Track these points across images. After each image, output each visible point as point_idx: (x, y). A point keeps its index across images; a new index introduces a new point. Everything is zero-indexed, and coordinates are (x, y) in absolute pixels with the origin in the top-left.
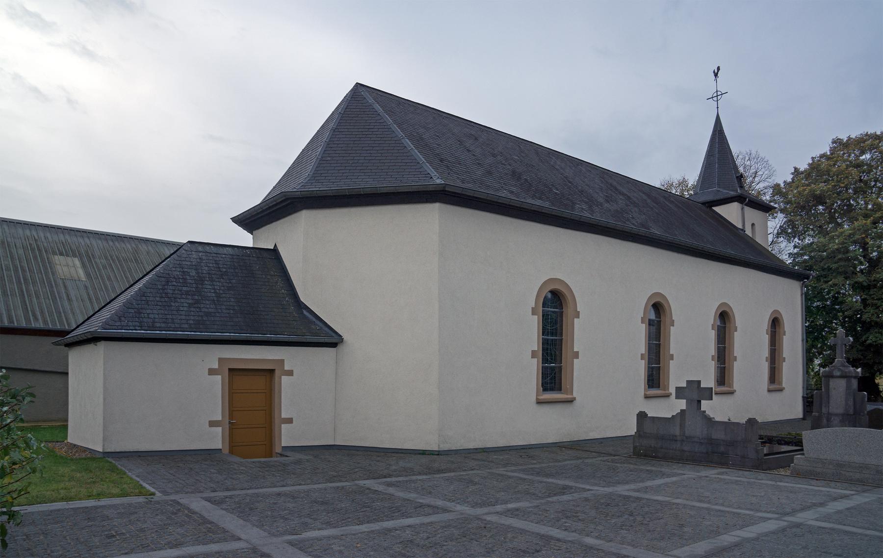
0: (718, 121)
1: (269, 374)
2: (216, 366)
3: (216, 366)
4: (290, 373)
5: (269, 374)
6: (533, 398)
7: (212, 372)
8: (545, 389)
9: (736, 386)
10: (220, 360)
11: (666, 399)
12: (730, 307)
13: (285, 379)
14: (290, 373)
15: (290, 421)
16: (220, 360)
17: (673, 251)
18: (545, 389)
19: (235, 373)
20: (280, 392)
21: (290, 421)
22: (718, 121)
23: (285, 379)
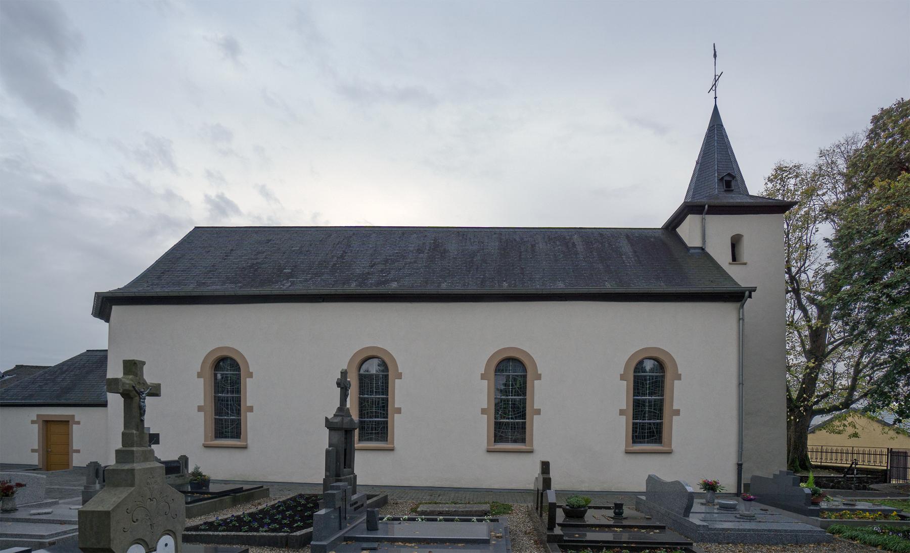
0: (716, 111)
1: (66, 423)
2: (35, 419)
3: (35, 419)
4: (78, 423)
5: (66, 423)
6: (623, 448)
7: (33, 422)
8: (634, 442)
9: (397, 444)
10: (38, 416)
11: (391, 453)
12: (204, 362)
13: (75, 426)
14: (78, 423)
15: (78, 451)
16: (38, 416)
17: (386, 301)
18: (634, 442)
19: (47, 424)
20: (532, 435)
21: (78, 451)
22: (716, 111)
23: (75, 426)
